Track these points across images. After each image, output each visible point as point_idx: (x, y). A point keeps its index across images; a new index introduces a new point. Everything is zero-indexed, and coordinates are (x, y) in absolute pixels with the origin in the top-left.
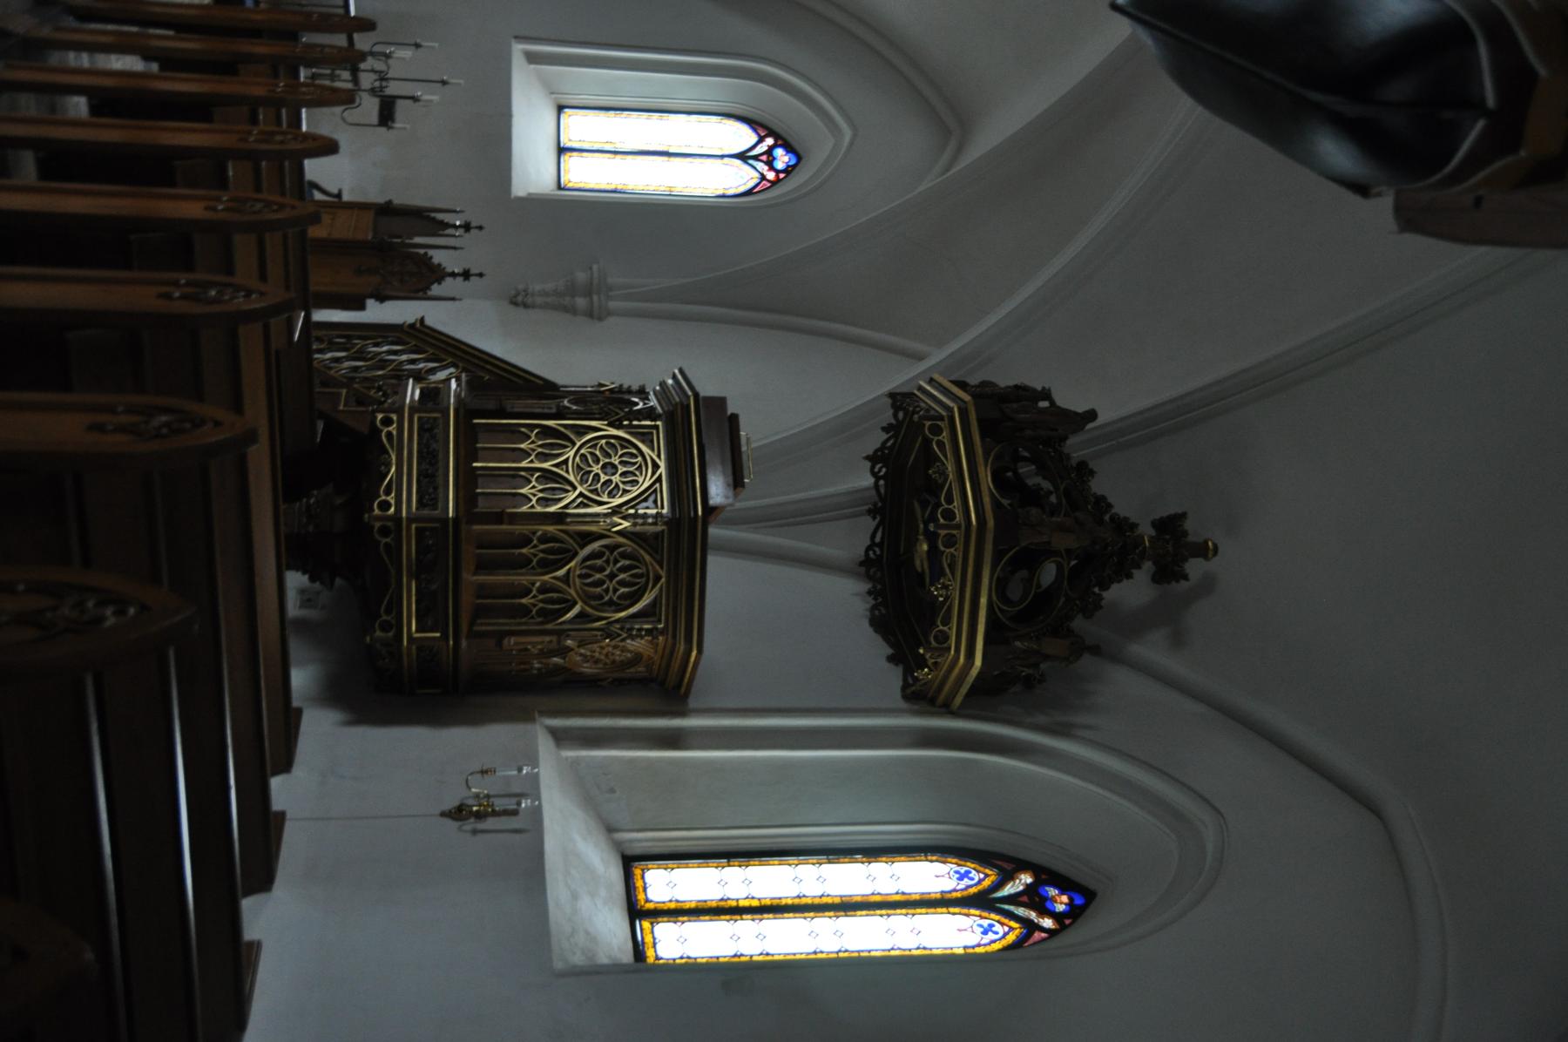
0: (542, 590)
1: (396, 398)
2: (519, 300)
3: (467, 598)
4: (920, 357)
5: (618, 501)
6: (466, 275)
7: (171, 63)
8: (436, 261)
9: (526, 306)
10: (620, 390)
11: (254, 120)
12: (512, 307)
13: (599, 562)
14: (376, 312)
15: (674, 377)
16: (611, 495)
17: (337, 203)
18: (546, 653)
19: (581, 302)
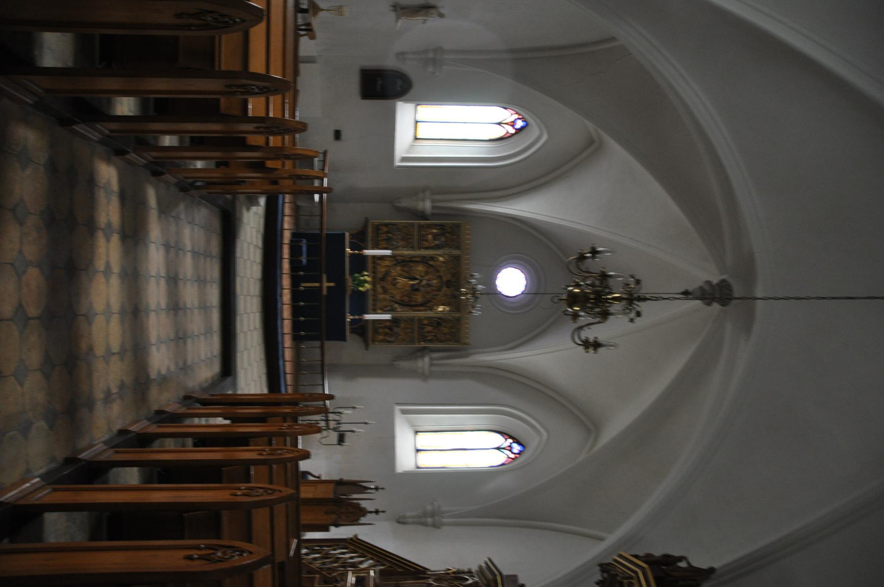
1: (342, 583)
2: (401, 521)
4: (601, 539)
6: (377, 512)
7: (236, 419)
8: (363, 506)
9: (404, 523)
10: (459, 572)
11: (270, 444)
12: (397, 524)
14: (335, 533)
15: (486, 564)
17: (320, 482)
19: (430, 520)
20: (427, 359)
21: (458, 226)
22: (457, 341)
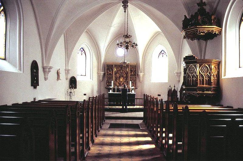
0: (206, 78)
3: (201, 86)
5: (195, 69)
6: (175, 87)
13: (203, 71)
16: (195, 70)
18: (214, 77)
20: (140, 74)
21: (107, 65)
22: (136, 66)
